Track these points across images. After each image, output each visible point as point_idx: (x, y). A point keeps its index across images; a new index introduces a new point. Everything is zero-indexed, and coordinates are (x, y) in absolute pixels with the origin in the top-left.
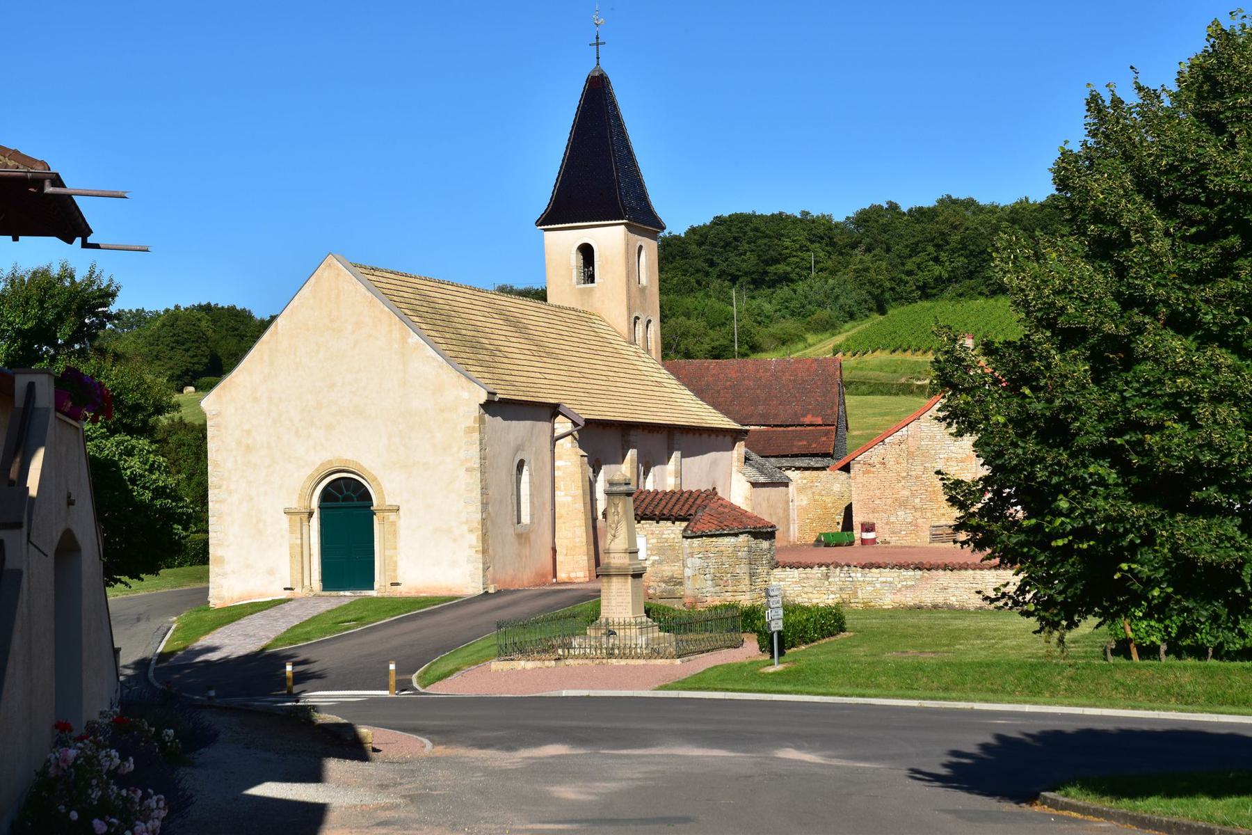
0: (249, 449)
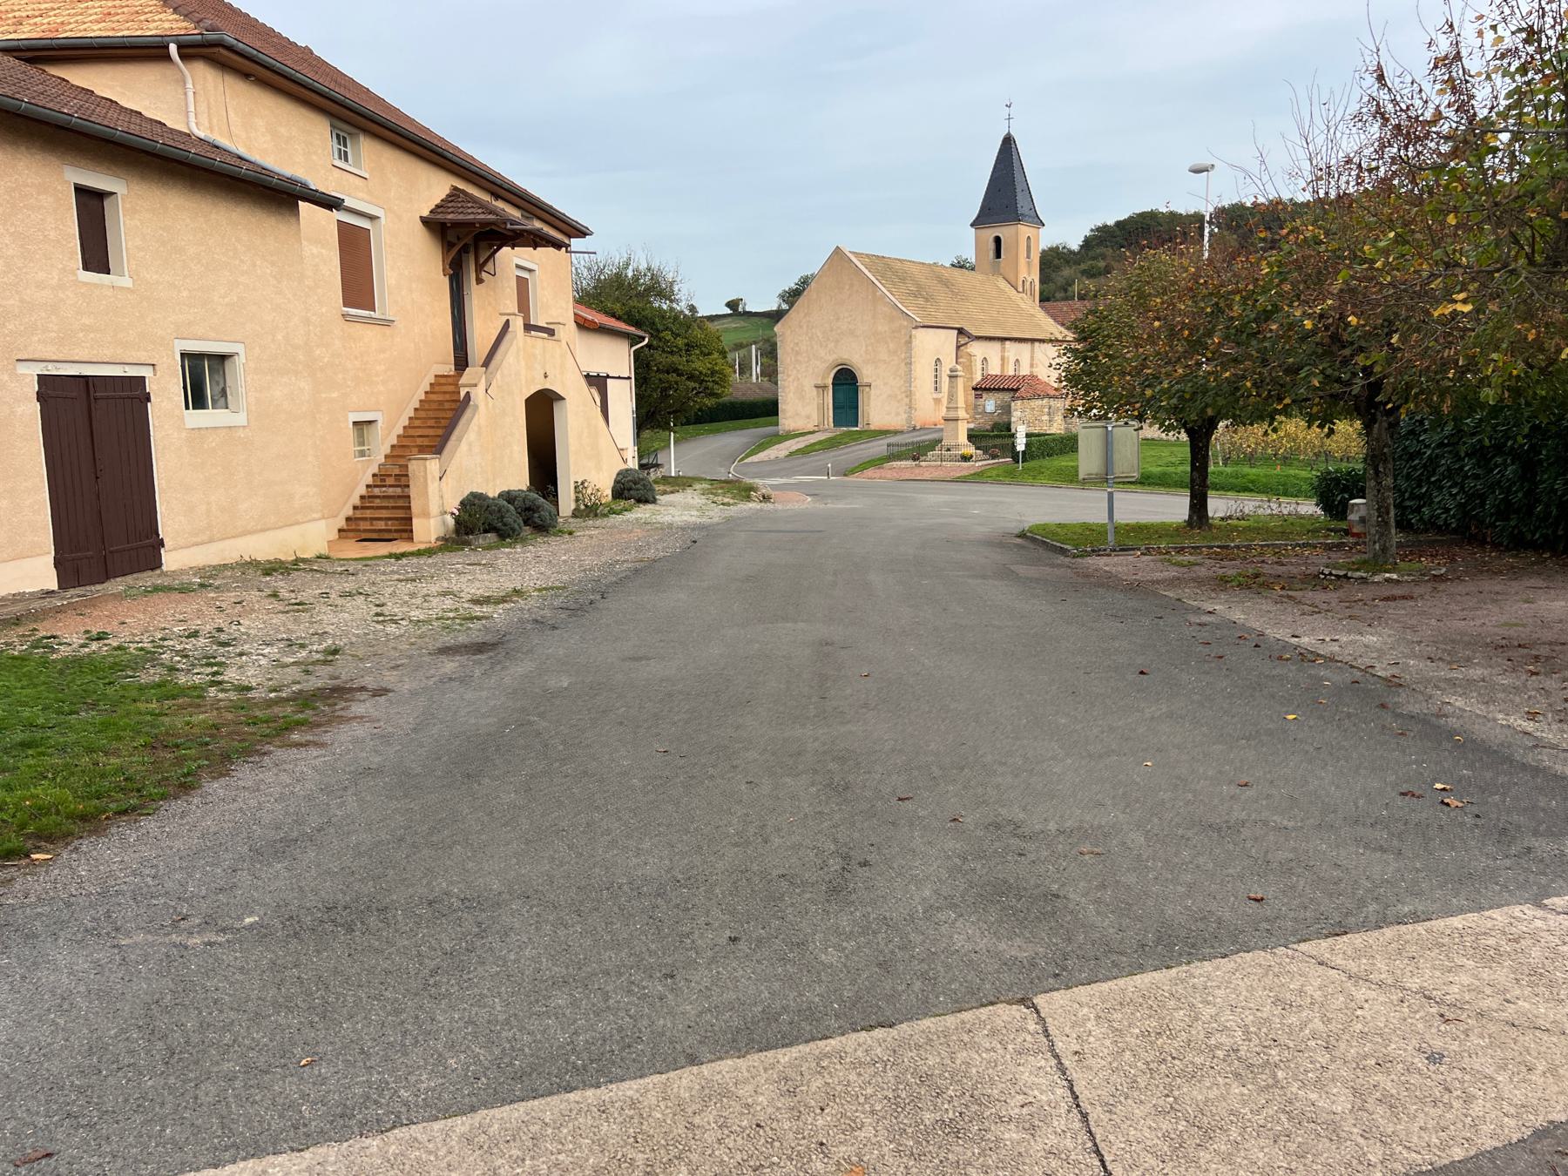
0: (798, 353)
